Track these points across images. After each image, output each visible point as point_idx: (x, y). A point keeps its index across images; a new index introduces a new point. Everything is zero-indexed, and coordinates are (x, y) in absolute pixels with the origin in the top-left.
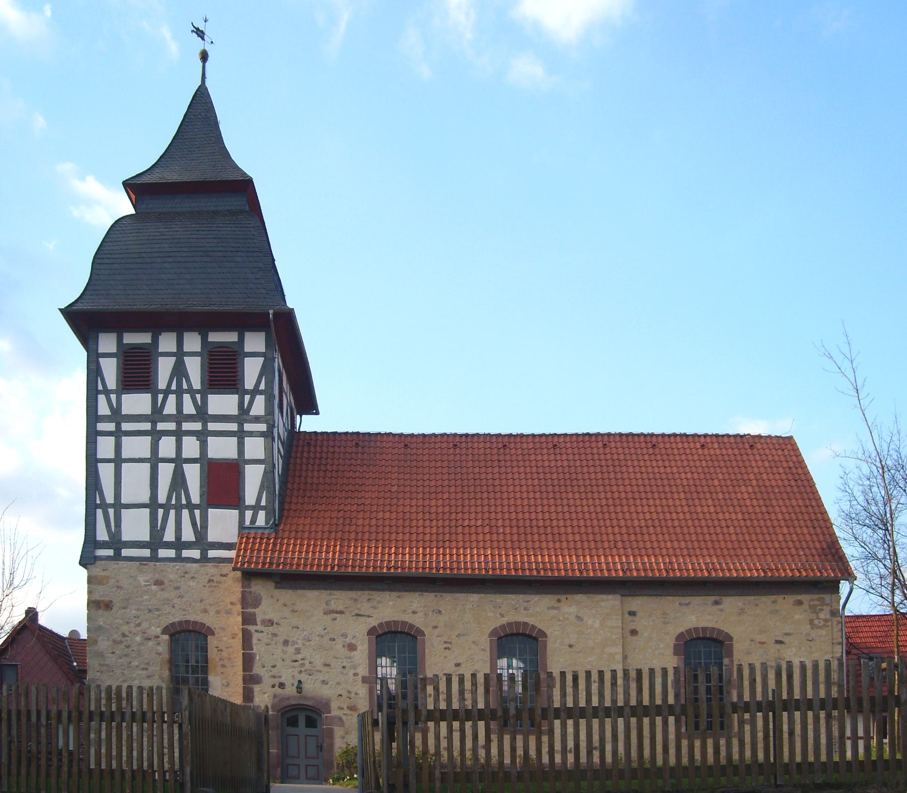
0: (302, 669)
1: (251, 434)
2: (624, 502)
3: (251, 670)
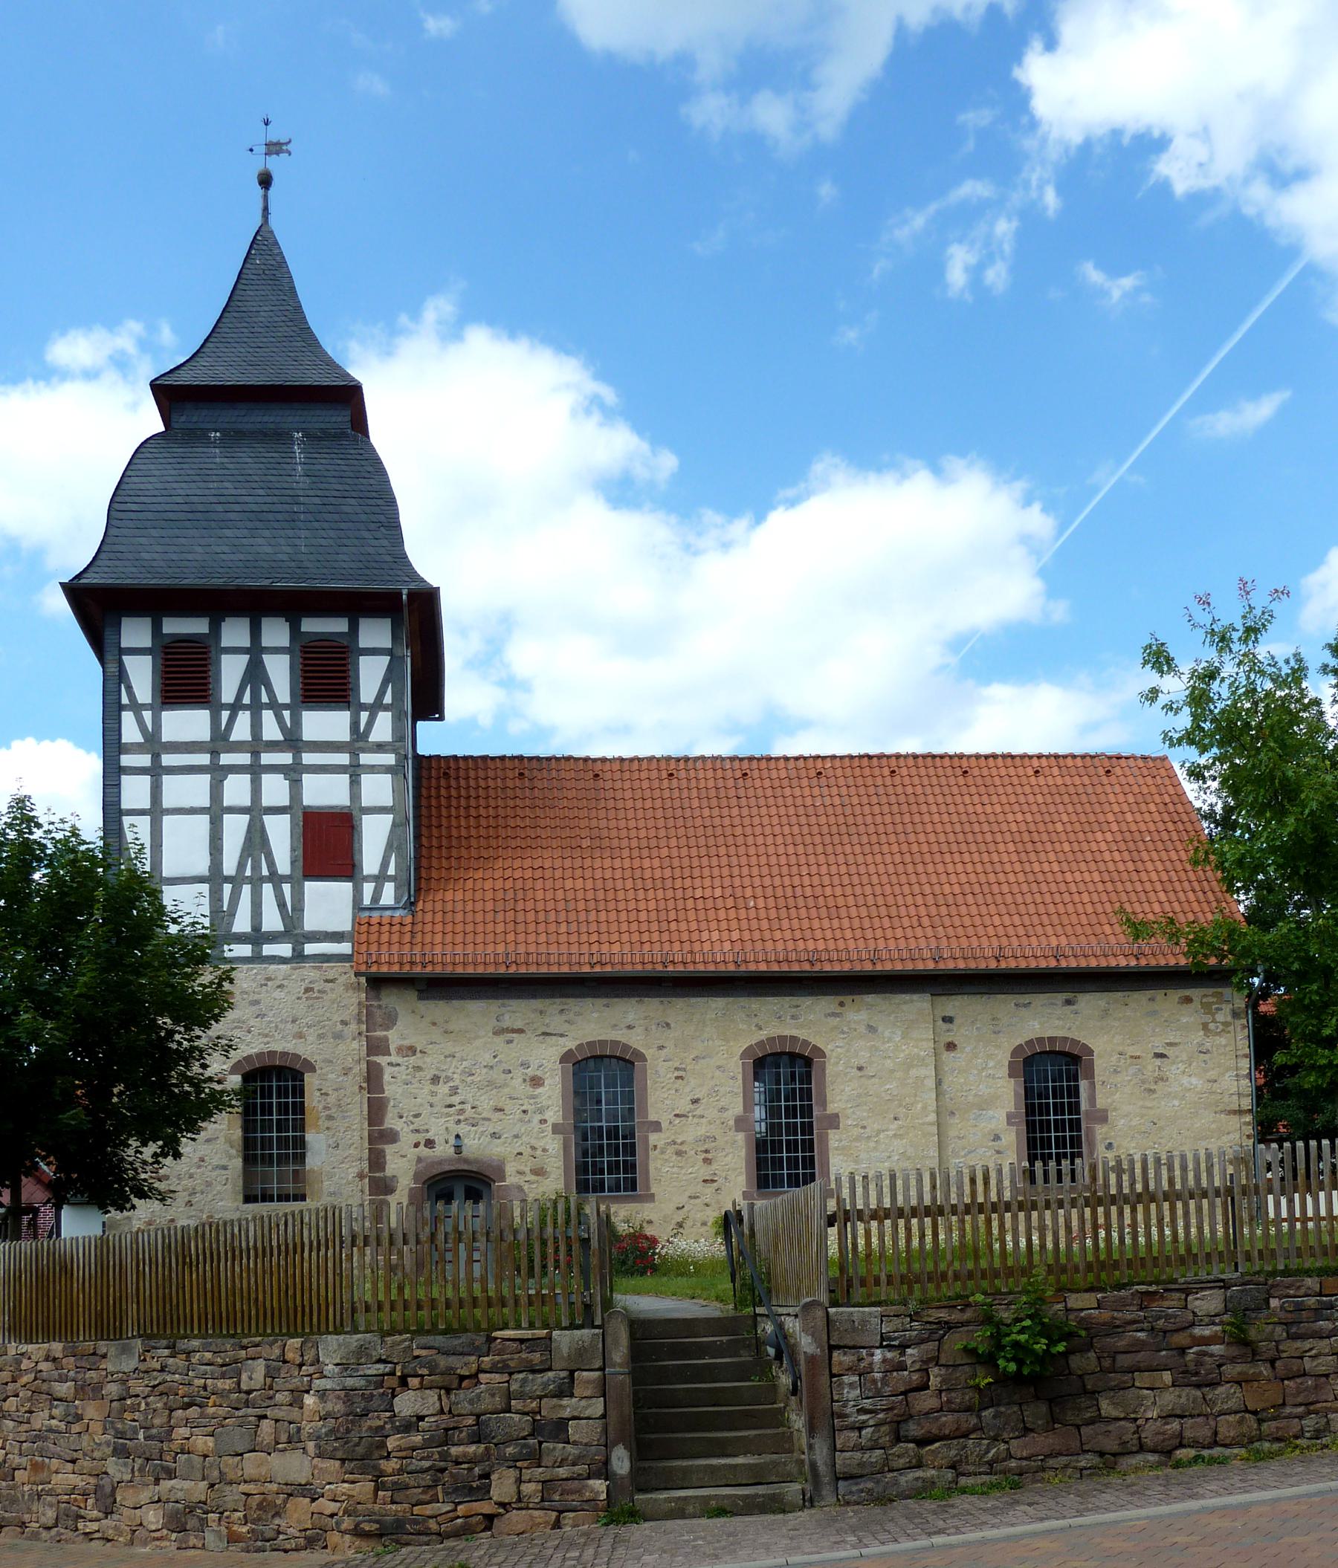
0: (462, 1118)
1: (373, 769)
2: (928, 858)
3: (381, 1123)
